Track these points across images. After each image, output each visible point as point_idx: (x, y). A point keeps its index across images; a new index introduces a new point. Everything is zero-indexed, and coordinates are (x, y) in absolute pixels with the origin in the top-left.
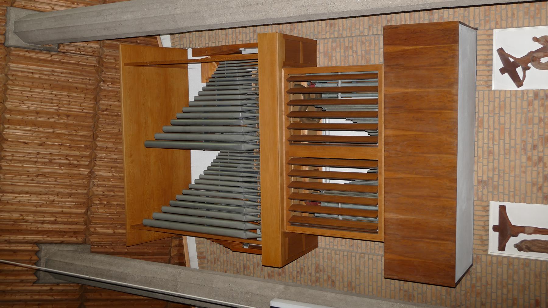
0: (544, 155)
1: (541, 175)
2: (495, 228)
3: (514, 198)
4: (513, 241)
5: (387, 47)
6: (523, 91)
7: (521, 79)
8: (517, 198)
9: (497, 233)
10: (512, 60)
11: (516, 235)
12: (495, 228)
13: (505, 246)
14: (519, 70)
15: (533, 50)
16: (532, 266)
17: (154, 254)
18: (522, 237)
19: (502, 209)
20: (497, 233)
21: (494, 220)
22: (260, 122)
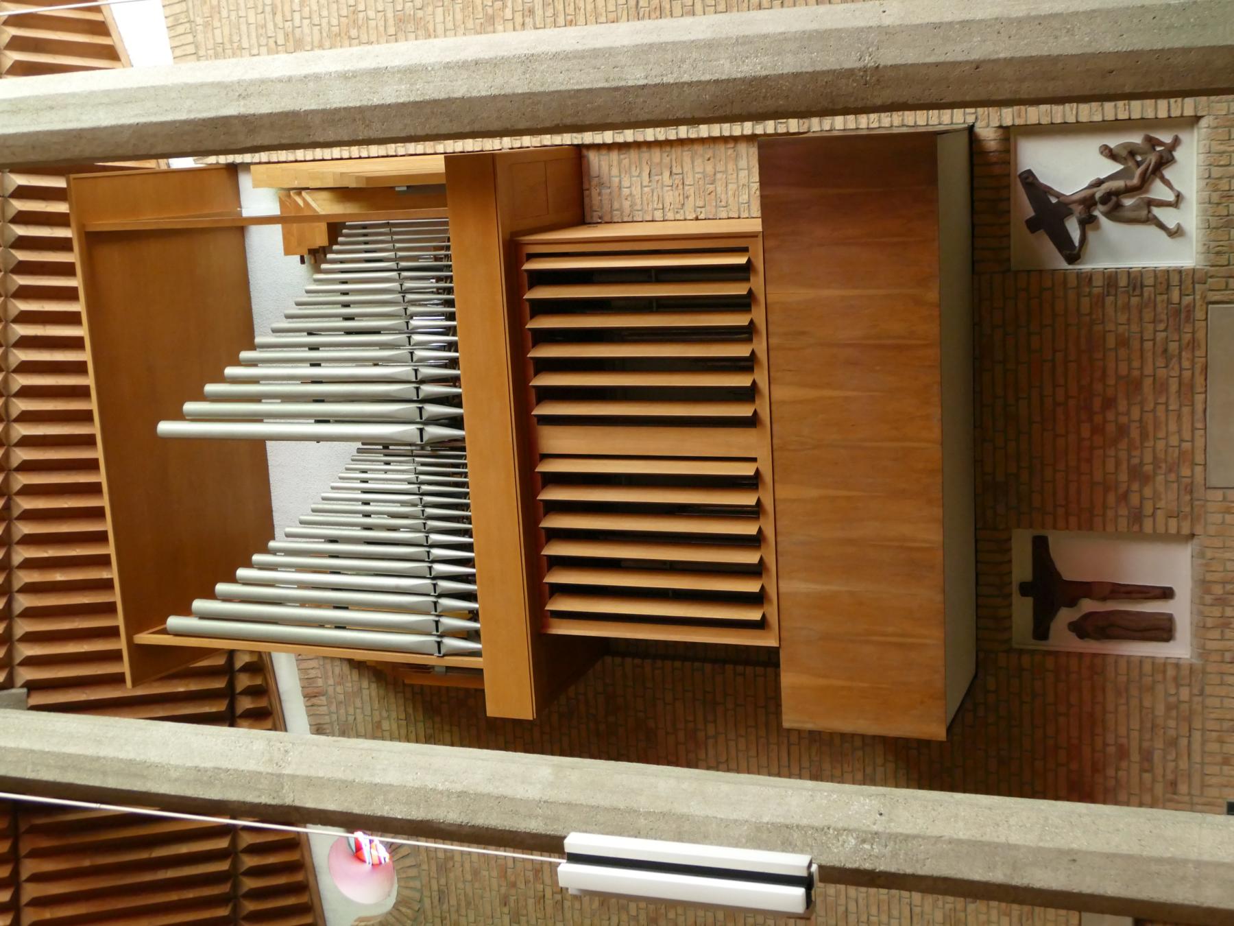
0: (1130, 421)
1: (1124, 466)
2: (1025, 589)
3: (1067, 522)
4: (1065, 616)
5: (479, 687)
6: (1079, 275)
7: (1077, 244)
8: (1073, 520)
9: (1029, 602)
10: (1054, 200)
11: (1072, 603)
12: (1025, 589)
13: (1048, 629)
14: (1073, 229)
15: (1103, 176)
16: (859, 776)
17: (65, 107)
18: (1088, 605)
19: (1040, 545)
20: (1029, 602)
21: (1022, 568)
22: (546, 30)
